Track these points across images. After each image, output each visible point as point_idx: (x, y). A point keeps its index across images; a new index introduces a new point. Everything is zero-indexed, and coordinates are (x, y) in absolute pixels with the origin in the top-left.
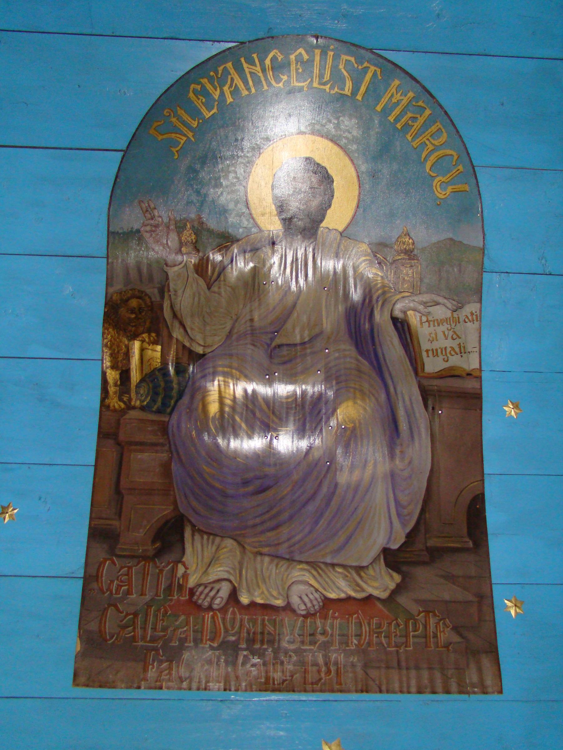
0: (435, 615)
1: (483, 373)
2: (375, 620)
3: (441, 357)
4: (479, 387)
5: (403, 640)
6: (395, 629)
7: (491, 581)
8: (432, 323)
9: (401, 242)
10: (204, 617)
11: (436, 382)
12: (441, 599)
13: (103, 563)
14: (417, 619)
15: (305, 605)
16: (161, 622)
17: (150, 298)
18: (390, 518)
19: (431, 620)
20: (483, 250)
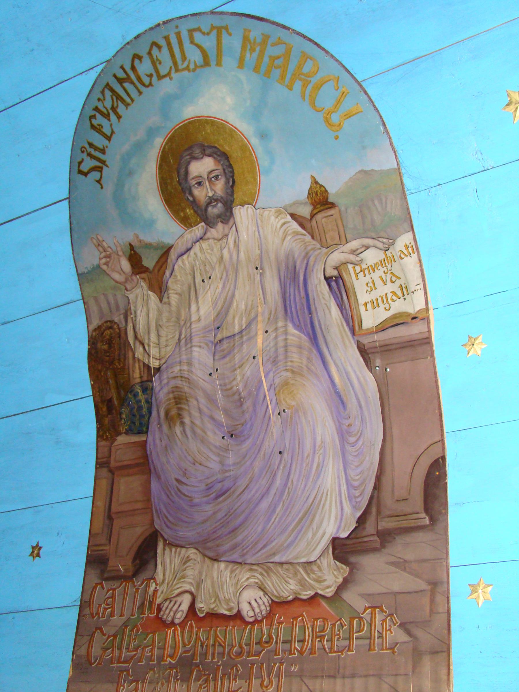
0: (382, 611)
1: (430, 312)
2: (319, 622)
3: (382, 306)
4: (426, 330)
5: (346, 643)
6: (339, 630)
7: (447, 563)
8: (366, 271)
9: (313, 193)
10: (167, 633)
11: (376, 337)
12: (390, 591)
13: (95, 588)
14: (362, 618)
15: (254, 610)
16: (134, 641)
17: (118, 325)
18: (341, 503)
19: (377, 615)
20: (398, 171)
